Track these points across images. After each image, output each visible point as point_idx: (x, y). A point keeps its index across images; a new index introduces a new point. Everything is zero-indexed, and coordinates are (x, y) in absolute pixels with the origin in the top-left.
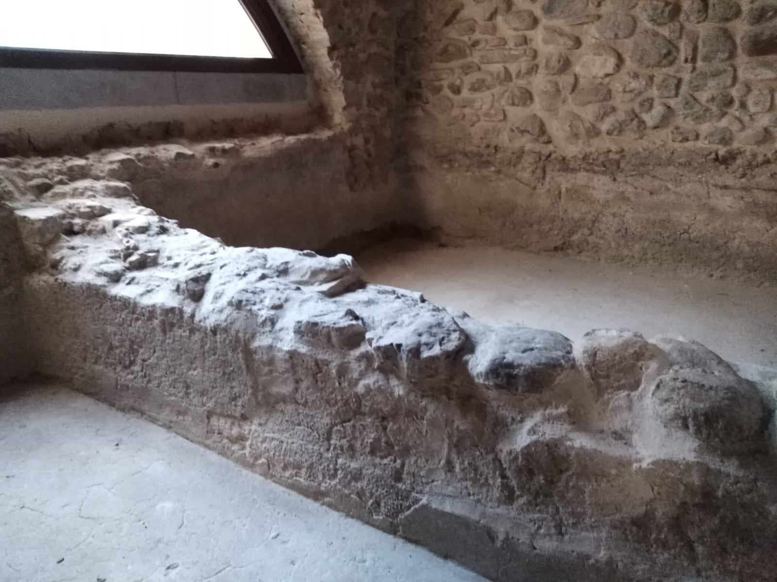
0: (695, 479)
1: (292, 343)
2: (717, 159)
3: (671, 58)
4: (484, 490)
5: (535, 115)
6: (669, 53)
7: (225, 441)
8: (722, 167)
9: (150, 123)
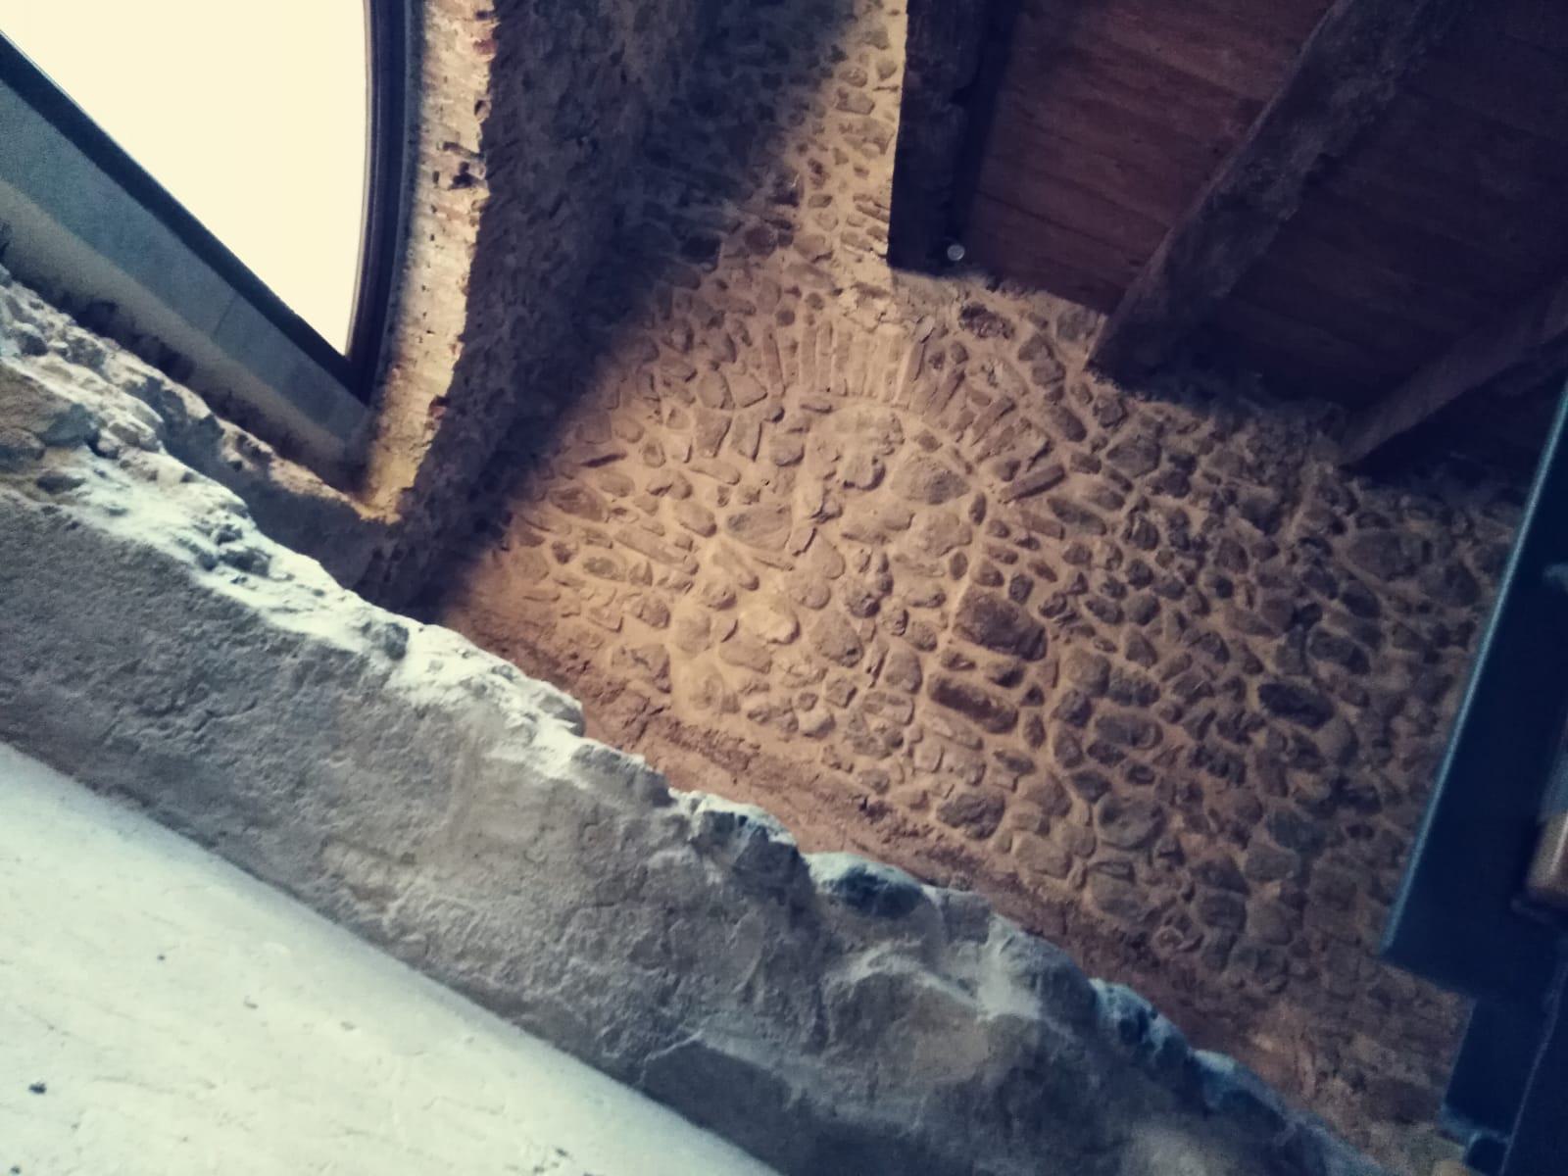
0: (1034, 1038)
1: (566, 770)
2: (863, 807)
3: (854, 658)
4: (789, 1030)
5: (662, 646)
6: (853, 652)
7: (344, 891)
8: (867, 821)
9: (156, 339)
